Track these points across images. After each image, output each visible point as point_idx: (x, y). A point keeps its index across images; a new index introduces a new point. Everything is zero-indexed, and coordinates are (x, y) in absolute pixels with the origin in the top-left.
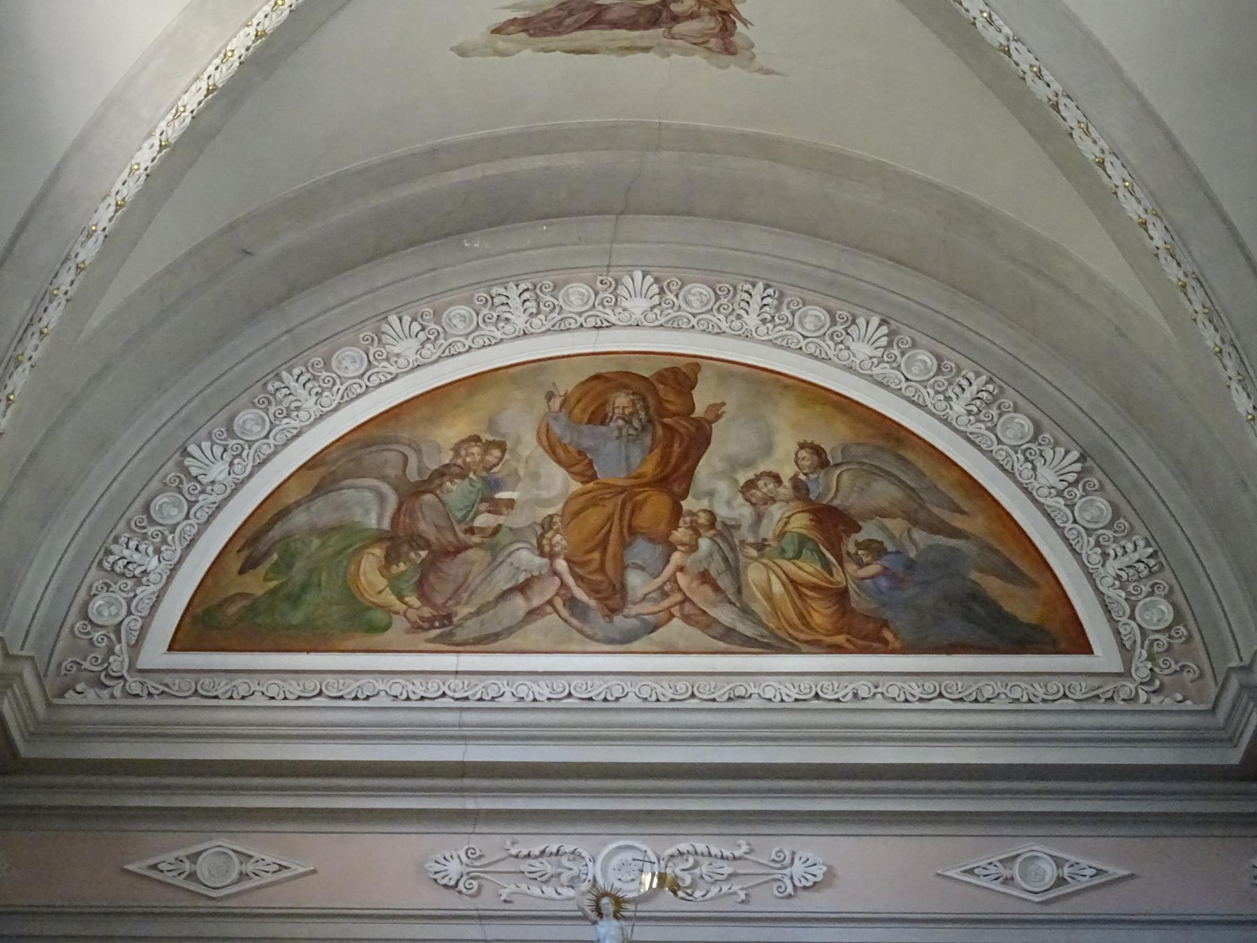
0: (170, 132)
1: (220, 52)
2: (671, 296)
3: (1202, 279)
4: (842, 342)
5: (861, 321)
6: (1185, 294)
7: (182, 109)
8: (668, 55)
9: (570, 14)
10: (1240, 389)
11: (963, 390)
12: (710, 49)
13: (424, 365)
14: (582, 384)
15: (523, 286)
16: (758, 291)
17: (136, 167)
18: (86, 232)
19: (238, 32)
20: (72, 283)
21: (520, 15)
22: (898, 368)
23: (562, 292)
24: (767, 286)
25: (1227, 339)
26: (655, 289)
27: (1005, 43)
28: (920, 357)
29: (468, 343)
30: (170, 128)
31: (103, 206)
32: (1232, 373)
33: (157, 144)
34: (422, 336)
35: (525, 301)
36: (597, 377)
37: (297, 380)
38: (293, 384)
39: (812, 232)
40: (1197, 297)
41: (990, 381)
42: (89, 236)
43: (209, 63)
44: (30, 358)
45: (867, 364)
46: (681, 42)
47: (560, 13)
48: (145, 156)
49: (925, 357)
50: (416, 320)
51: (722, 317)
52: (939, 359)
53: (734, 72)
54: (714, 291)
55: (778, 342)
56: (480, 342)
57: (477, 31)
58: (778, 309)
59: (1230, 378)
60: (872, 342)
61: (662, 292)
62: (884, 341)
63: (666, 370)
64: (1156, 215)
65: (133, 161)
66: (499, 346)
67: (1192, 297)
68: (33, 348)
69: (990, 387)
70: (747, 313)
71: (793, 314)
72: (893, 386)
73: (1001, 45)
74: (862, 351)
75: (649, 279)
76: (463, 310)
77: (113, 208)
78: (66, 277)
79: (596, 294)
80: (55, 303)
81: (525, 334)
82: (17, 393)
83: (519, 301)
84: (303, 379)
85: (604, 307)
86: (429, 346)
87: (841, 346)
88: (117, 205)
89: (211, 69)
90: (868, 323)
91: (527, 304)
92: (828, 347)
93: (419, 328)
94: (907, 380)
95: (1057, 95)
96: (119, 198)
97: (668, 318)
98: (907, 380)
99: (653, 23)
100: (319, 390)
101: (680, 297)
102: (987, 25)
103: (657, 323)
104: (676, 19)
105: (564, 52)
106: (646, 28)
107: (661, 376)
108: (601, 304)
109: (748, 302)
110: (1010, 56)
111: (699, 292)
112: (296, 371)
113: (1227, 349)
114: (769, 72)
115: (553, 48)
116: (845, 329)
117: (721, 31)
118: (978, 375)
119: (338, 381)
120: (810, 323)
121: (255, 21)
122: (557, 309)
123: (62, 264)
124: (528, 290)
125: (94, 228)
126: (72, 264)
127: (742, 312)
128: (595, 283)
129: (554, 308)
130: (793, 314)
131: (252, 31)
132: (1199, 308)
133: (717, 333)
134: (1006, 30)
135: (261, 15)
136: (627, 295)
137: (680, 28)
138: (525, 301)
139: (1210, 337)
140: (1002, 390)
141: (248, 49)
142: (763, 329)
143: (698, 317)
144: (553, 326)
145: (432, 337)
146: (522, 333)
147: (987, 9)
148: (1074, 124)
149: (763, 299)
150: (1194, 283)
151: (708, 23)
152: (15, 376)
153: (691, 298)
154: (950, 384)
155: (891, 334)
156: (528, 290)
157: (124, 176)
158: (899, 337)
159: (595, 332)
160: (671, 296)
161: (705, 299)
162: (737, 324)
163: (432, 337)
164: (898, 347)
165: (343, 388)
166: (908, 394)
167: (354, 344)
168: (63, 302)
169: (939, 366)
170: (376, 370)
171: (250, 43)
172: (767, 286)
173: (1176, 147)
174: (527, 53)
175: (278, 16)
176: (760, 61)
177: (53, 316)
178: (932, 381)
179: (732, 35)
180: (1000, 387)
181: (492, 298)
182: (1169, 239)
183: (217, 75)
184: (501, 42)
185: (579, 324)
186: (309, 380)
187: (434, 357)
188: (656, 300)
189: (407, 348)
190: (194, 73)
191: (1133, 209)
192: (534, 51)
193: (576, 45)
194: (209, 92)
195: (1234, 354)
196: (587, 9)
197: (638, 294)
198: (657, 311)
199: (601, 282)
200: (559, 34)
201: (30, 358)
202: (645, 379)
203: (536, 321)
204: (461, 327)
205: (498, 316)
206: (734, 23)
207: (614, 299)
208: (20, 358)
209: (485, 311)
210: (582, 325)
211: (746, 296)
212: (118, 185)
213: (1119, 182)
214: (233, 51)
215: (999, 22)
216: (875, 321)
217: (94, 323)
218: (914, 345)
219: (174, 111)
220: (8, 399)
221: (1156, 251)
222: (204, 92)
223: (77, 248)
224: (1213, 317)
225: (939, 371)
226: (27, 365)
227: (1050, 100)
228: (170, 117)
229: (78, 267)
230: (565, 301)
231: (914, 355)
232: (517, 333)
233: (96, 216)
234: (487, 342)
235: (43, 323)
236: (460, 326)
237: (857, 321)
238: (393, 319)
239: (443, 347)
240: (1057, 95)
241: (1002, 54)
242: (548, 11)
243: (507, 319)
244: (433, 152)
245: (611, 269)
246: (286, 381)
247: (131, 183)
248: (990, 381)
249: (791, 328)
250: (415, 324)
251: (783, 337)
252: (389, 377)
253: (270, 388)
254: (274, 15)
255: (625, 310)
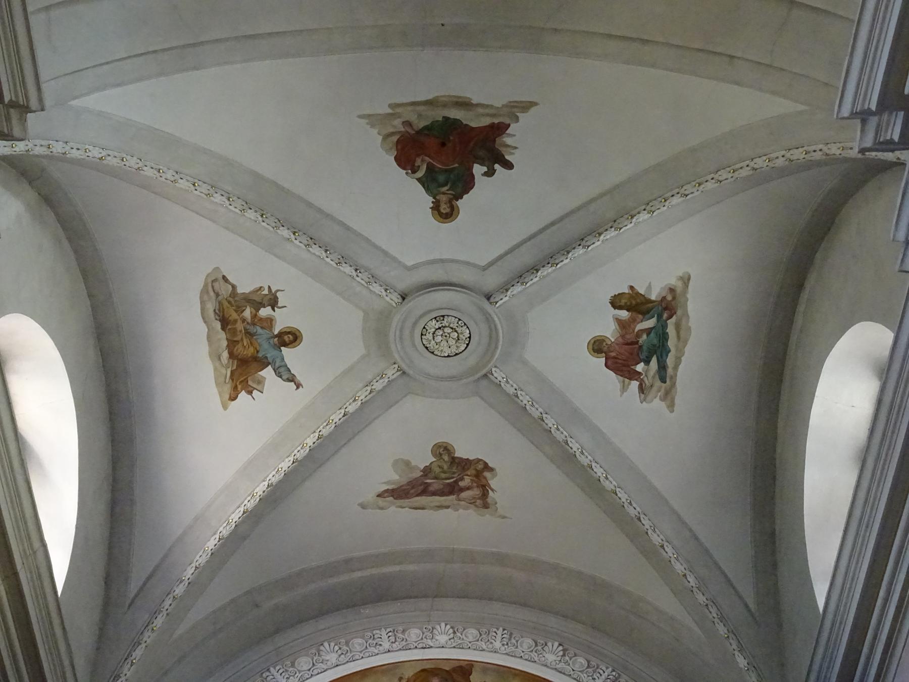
0: (224, 532)
1: (251, 494)
2: (459, 634)
3: (714, 601)
4: (541, 654)
5: (550, 644)
6: (708, 609)
7: (231, 521)
8: (458, 510)
9: (413, 488)
10: (740, 655)
11: (601, 675)
12: (476, 506)
13: (340, 665)
14: (416, 673)
15: (388, 630)
16: (500, 632)
17: (207, 549)
18: (180, 581)
19: (260, 483)
20: (170, 605)
21: (390, 487)
22: (569, 665)
23: (407, 632)
24: (504, 630)
25: (730, 630)
26: (451, 631)
27: (614, 488)
28: (579, 660)
29: (362, 655)
30: (225, 531)
31: (189, 568)
32: (734, 646)
33: (218, 537)
34: (340, 652)
35: (389, 637)
36: (423, 670)
37: (278, 672)
38: (275, 673)
39: (524, 605)
40: (714, 610)
41: (613, 671)
42: (181, 582)
43: (246, 499)
44: (146, 642)
45: (554, 663)
46: (463, 502)
47: (408, 487)
48: (212, 544)
49: (581, 660)
50: (337, 645)
51: (483, 643)
52: (588, 662)
53: (487, 518)
54: (479, 632)
55: (511, 654)
56: (367, 654)
57: (370, 496)
58: (510, 639)
59: (734, 650)
60: (552, 652)
61: (454, 632)
62: (561, 653)
63: (457, 667)
64: (690, 571)
65: (206, 546)
66: (377, 656)
67: (711, 610)
68: (149, 637)
69: (614, 673)
70: (495, 641)
71: (517, 641)
72: (566, 673)
73: (612, 490)
74: (550, 658)
75: (448, 627)
76: (360, 641)
77: (194, 569)
78: (168, 602)
79: (423, 633)
80: (161, 615)
81: (389, 651)
82: (137, 659)
83: (387, 637)
84: (281, 671)
85: (427, 639)
86: (343, 656)
87: (541, 656)
88: (196, 567)
89: (246, 502)
90: (553, 646)
91: (390, 638)
92: (534, 656)
93: (338, 648)
94: (573, 670)
95: (639, 513)
96: (197, 564)
97: (457, 644)
98: (573, 670)
99: (451, 493)
100: (288, 676)
101: (463, 635)
102: (605, 480)
103: (452, 646)
104: (462, 490)
105: (410, 508)
106: (447, 496)
107: (454, 670)
108: (426, 638)
109: (495, 637)
110: (617, 495)
111: (472, 633)
112: (278, 668)
113: (731, 635)
114: (504, 517)
115: (404, 506)
116: (542, 648)
117: (482, 496)
118: (607, 668)
119: (298, 672)
120: (525, 646)
121: (268, 479)
122: (405, 640)
123: (167, 596)
124: (391, 632)
125: (184, 578)
126: (171, 596)
127: (493, 641)
128: (423, 628)
129: (403, 639)
130: (517, 641)
131: (266, 483)
132: (715, 615)
133: (481, 650)
134: (614, 483)
135: (271, 476)
136: (438, 634)
137: (464, 495)
138: (389, 637)
139: (722, 630)
140: (619, 675)
141: (264, 492)
142: (503, 648)
143: (472, 643)
144: (403, 647)
145: (344, 653)
146: (387, 650)
147: (605, 472)
148: (648, 527)
149: (502, 635)
150: (712, 604)
151: (476, 492)
152: (137, 651)
153: (468, 635)
154: (594, 672)
155: (564, 650)
156: (391, 632)
157: (200, 553)
158: (568, 652)
159: (423, 650)
160: (459, 634)
161: (475, 636)
162: (490, 646)
163: (344, 653)
164: (568, 656)
165: (300, 675)
166: (574, 677)
167: (307, 655)
168: (165, 615)
169: (588, 665)
170: (317, 667)
171: (265, 489)
172: (504, 630)
173: (697, 539)
174: (393, 508)
175: (278, 477)
176: (501, 511)
177: (159, 622)
178: (585, 671)
179: (487, 497)
180: (618, 674)
181: (374, 635)
182: (697, 583)
183: (249, 505)
184: (381, 502)
185: (415, 646)
186: (283, 672)
187: (345, 661)
188: (452, 636)
189: (333, 658)
190: (238, 504)
191: (679, 567)
192: (396, 507)
193: (417, 505)
194: (244, 512)
195: (734, 638)
196: (421, 485)
197: (443, 633)
198: (452, 640)
199: (426, 628)
200: (408, 498)
201: (146, 642)
202: (447, 671)
203: (394, 645)
204: (358, 648)
205: (376, 644)
206: (488, 491)
207: (431, 636)
208: (141, 642)
209: (370, 641)
210: (416, 647)
211: (494, 634)
212: (198, 557)
213: (671, 555)
214: (257, 493)
215: (611, 479)
216: (556, 644)
217: (179, 632)
218: (575, 655)
219: (227, 522)
220: (132, 662)
221: (692, 589)
222: (242, 512)
223: (175, 588)
224: (722, 619)
225: (588, 667)
226: (143, 645)
227: (636, 516)
228: (225, 525)
229: (174, 597)
230: (408, 636)
231: (576, 660)
232: (385, 651)
233: (185, 574)
234: (371, 654)
235: (154, 625)
236: (358, 648)
237: (548, 644)
238: (326, 644)
239: (349, 657)
240: (639, 513)
241: (613, 494)
242: (402, 486)
243: (380, 645)
244: (347, 561)
245: (430, 623)
246: (272, 672)
247: (204, 556)
248: (613, 671)
249: (517, 647)
250: (336, 647)
251: (513, 651)
252: (323, 670)
253: (264, 675)
254: (277, 476)
255: (437, 640)
